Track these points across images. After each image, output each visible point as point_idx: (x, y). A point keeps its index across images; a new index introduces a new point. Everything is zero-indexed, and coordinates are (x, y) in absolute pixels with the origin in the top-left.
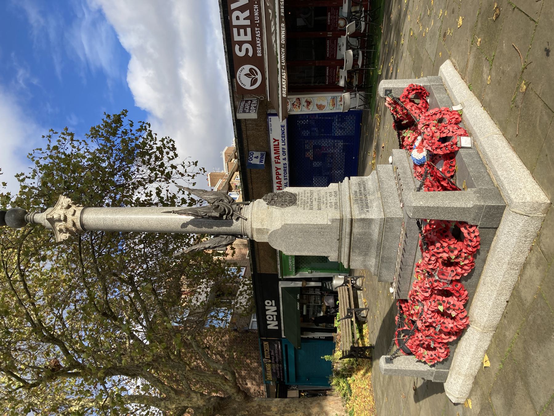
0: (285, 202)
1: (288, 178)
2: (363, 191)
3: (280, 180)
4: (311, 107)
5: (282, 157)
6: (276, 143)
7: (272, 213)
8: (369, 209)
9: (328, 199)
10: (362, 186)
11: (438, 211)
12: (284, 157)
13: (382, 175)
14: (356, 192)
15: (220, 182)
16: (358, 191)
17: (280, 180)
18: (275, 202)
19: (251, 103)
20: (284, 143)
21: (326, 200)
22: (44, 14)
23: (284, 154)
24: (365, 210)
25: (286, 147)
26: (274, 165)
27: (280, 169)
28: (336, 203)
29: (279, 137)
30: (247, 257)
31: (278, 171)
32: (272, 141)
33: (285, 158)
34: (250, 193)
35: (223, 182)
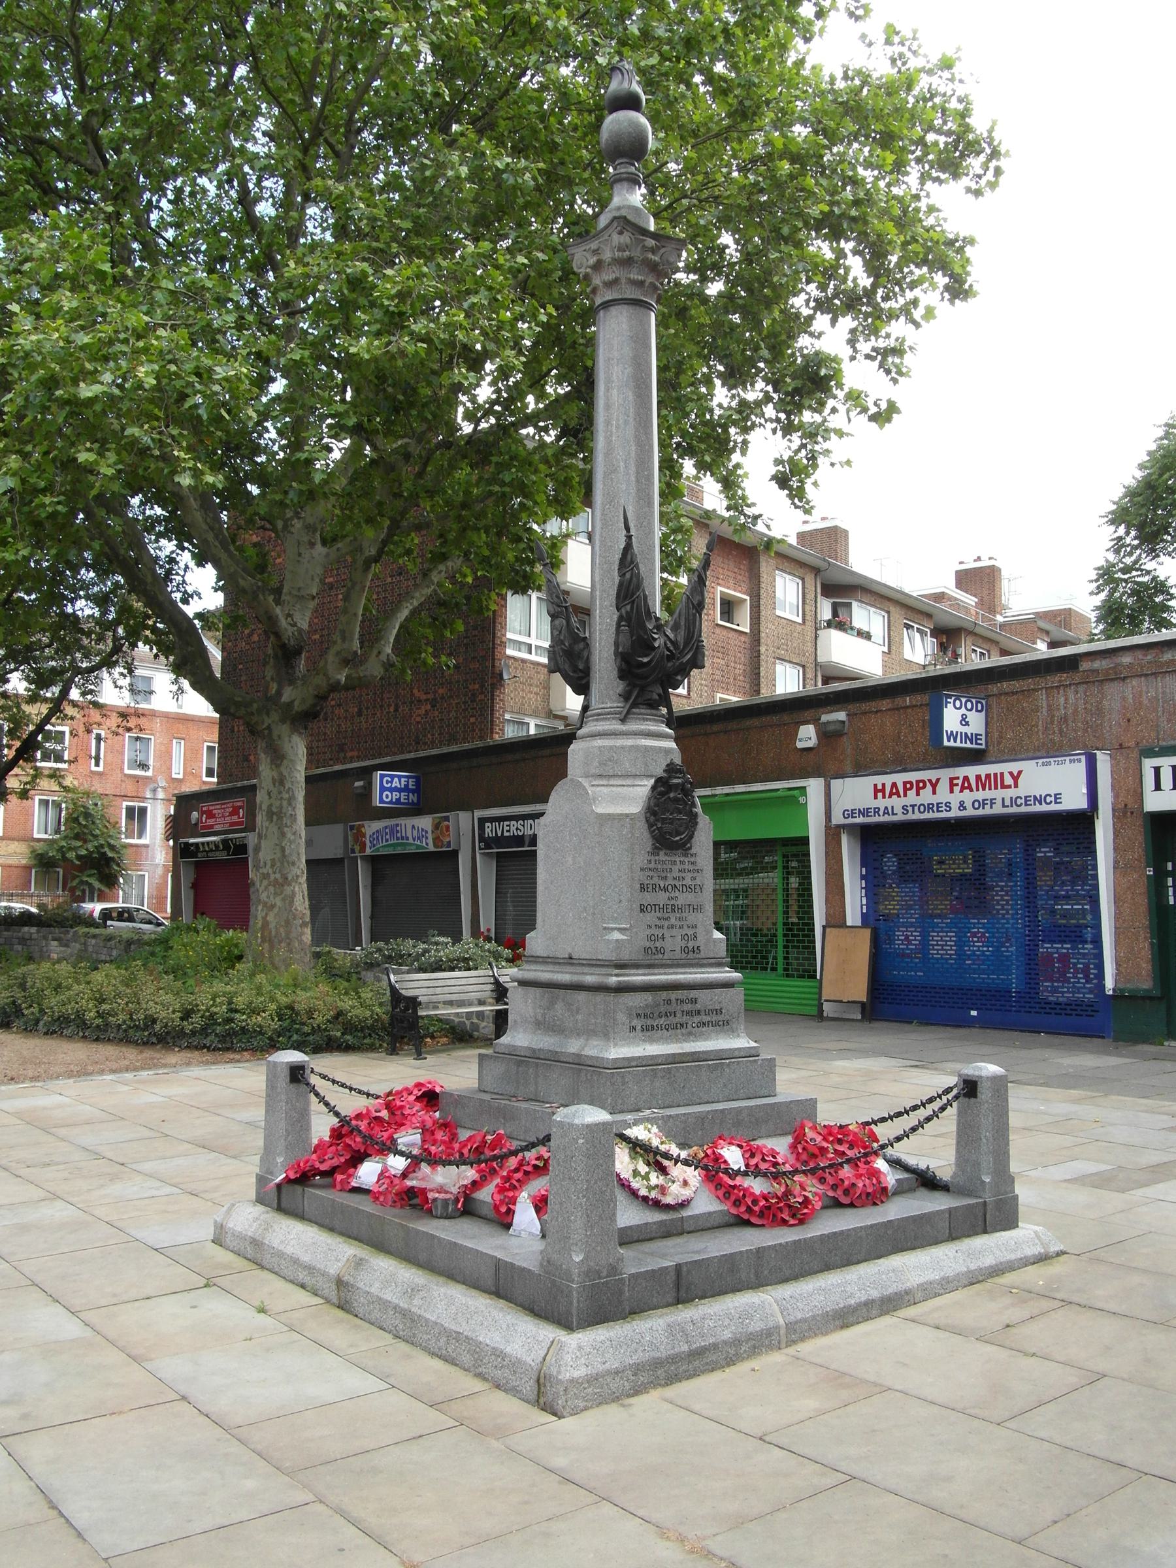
2: (696, 1019)
3: (974, 786)
5: (968, 797)
6: (1008, 780)
9: (674, 932)
11: (563, 1179)
12: (968, 805)
14: (694, 1001)
15: (970, 600)
16: (698, 1006)
17: (974, 786)
20: (1007, 802)
21: (672, 927)
23: (976, 805)
24: (637, 1023)
25: (998, 809)
26: (944, 774)
27: (934, 793)
28: (660, 951)
29: (1023, 790)
30: (719, 695)
31: (929, 787)
32: (1014, 767)
33: (965, 808)
34: (865, 706)
35: (967, 610)
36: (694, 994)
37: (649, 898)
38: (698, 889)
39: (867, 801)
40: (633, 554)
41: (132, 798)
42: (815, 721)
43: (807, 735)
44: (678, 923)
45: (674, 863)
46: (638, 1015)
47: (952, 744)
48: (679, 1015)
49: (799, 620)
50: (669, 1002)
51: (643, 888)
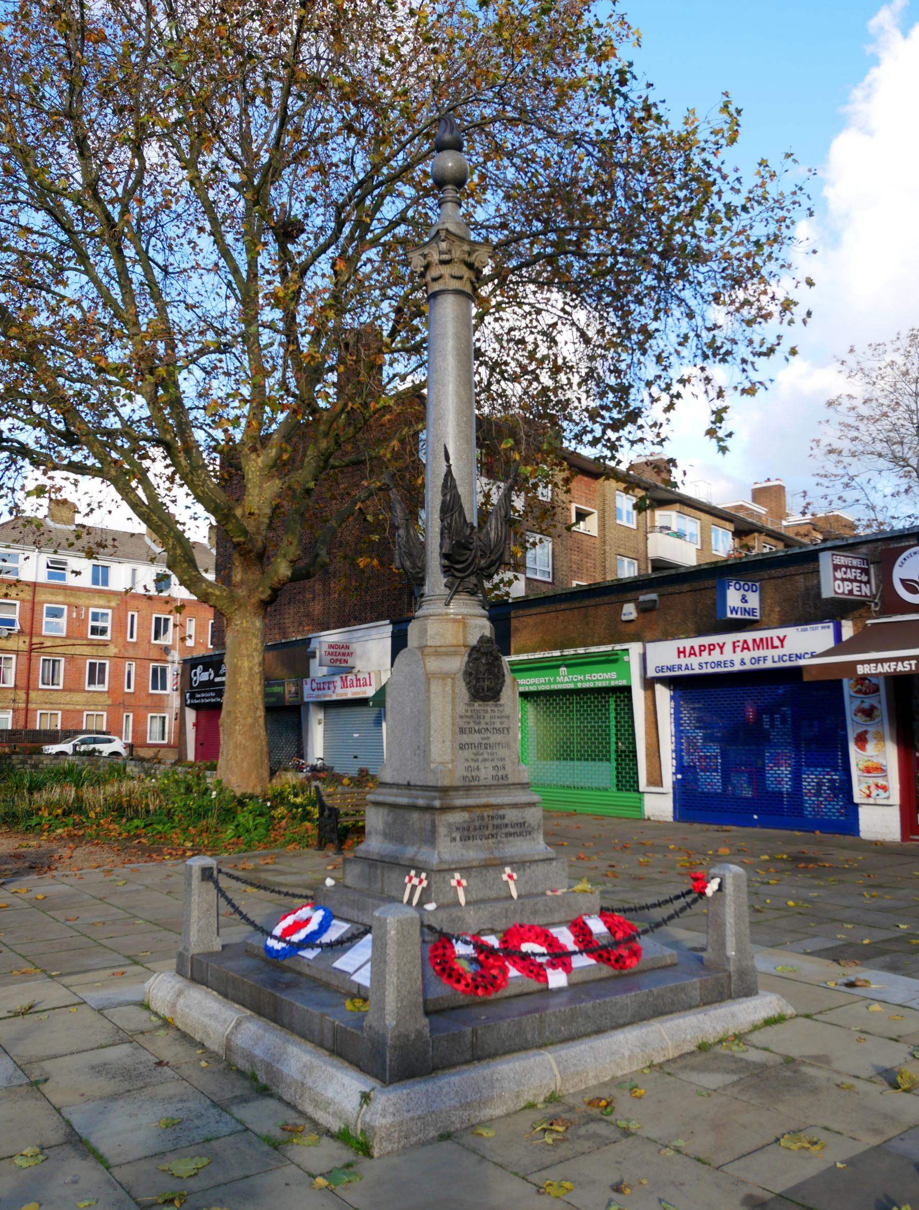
0: (478, 680)
1: (704, 671)
2: (504, 830)
3: (697, 652)
4: (860, 718)
5: (747, 655)
6: (777, 643)
7: (454, 654)
8: (458, 843)
9: (487, 764)
10: (518, 830)
12: (747, 661)
13: (540, 870)
14: (503, 817)
15: (762, 510)
16: (506, 821)
17: (697, 652)
18: (476, 659)
19: (861, 582)
20: (776, 659)
22: (309, 343)
25: (769, 664)
26: (728, 639)
28: (476, 778)
29: (790, 647)
31: (718, 649)
32: (781, 632)
34: (671, 589)
37: (466, 738)
39: (673, 660)
40: (453, 479)
41: (156, 661)
42: (635, 600)
43: (629, 611)
44: (490, 757)
45: (486, 711)
46: (458, 829)
47: (734, 616)
48: (490, 827)
49: (634, 527)
50: (482, 818)
51: (462, 731)
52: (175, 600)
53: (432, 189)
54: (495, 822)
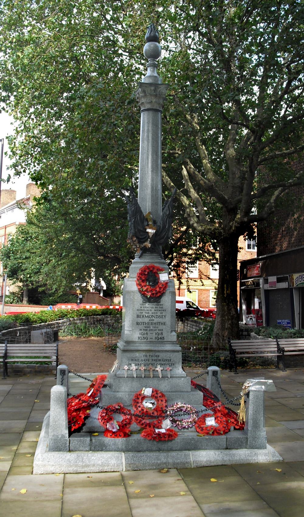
16: (160, 358)
36: (157, 354)
37: (140, 320)
38: (163, 317)
52: (139, 289)
53: (259, 59)
54: (154, 358)
